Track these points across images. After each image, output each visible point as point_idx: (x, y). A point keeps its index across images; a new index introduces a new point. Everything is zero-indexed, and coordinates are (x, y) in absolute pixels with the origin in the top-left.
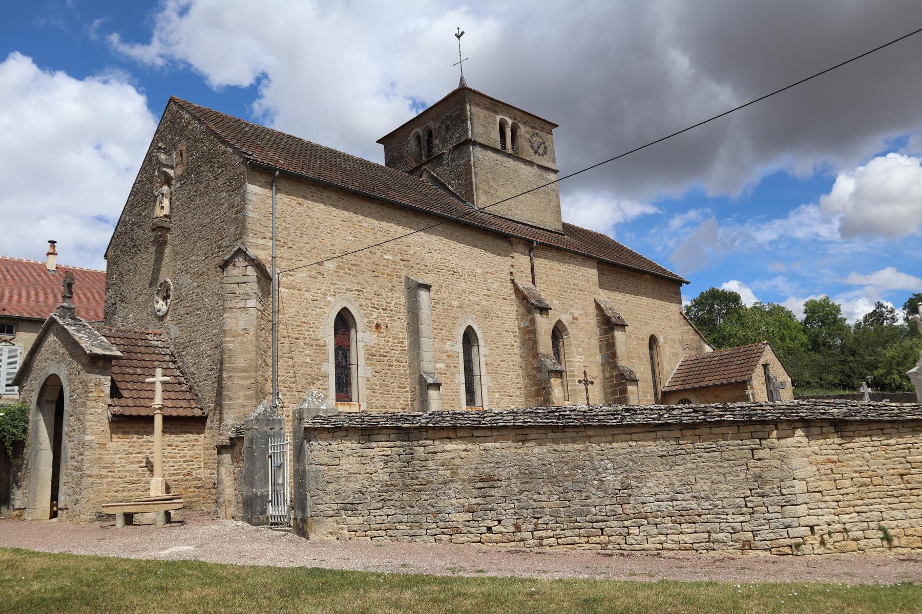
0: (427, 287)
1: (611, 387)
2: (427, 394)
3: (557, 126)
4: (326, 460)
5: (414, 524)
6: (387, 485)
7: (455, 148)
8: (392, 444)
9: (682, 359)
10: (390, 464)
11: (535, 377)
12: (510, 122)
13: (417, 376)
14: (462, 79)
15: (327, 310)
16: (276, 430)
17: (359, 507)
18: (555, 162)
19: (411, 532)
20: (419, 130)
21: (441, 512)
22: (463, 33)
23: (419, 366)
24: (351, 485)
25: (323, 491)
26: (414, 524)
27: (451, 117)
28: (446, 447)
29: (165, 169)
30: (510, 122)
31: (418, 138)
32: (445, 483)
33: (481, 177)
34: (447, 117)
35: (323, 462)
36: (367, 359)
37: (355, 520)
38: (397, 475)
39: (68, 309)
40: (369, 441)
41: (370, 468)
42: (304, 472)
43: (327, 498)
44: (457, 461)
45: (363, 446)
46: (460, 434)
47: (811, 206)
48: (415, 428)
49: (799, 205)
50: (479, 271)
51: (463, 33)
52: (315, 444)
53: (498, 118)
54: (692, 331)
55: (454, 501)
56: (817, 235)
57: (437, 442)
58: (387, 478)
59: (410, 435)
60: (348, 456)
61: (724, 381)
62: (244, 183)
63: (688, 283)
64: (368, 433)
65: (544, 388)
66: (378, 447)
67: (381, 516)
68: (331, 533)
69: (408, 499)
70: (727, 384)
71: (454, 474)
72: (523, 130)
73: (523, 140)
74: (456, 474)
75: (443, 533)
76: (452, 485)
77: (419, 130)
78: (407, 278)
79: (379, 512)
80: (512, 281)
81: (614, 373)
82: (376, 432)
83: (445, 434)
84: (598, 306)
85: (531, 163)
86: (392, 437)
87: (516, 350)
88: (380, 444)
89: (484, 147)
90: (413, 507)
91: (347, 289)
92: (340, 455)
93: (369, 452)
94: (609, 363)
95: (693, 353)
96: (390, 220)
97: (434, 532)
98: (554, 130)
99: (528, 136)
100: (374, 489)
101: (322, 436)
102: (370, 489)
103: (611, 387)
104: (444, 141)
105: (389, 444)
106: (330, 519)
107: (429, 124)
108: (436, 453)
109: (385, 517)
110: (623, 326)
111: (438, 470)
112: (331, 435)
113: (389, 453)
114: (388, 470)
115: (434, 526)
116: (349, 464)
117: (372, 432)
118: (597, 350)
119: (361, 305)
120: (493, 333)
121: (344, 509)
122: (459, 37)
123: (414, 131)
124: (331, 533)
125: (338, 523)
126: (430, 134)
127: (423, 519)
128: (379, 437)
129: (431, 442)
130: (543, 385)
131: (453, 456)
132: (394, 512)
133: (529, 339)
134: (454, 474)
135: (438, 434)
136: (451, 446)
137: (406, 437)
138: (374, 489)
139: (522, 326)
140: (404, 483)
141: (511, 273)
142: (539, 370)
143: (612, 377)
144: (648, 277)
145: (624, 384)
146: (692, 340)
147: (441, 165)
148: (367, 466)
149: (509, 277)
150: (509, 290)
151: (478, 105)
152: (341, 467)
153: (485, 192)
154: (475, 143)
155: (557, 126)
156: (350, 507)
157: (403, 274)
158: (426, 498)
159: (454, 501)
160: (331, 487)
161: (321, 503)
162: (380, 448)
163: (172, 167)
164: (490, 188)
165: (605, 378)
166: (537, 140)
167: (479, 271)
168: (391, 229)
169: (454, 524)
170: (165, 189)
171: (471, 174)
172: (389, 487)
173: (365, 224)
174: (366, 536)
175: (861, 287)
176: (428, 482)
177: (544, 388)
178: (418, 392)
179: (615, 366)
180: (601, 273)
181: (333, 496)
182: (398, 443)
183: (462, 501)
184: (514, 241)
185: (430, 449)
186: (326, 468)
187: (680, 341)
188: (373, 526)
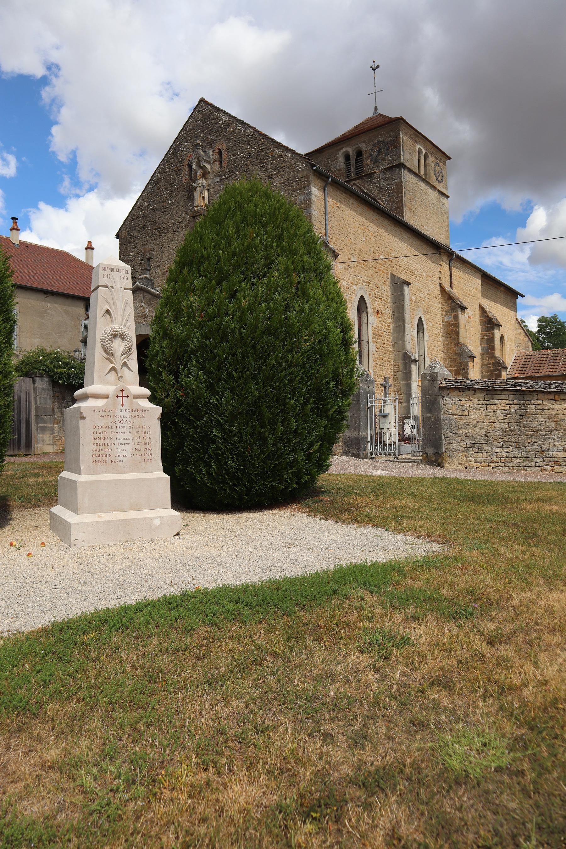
0: (408, 284)
1: (488, 371)
2: (410, 368)
3: (450, 158)
4: (457, 412)
5: (528, 458)
6: (506, 431)
7: (386, 169)
8: (510, 402)
9: (515, 355)
10: (509, 416)
11: (455, 360)
12: (424, 151)
13: (401, 353)
14: (376, 109)
15: (353, 296)
16: (371, 388)
17: (484, 446)
18: (447, 189)
19: (524, 464)
20: (349, 150)
21: (547, 451)
22: (378, 66)
23: (404, 345)
24: (478, 430)
25: (455, 434)
26: (525, 459)
27: (383, 142)
28: (551, 406)
29: (205, 164)
30: (424, 151)
31: (347, 158)
32: (551, 431)
33: (407, 196)
34: (379, 142)
35: (455, 413)
36: (373, 338)
37: (480, 455)
38: (514, 424)
39: (150, 280)
40: (493, 399)
41: (493, 418)
42: (438, 421)
43: (458, 439)
44: (560, 416)
45: (487, 402)
46: (562, 398)
47: (500, 239)
48: (530, 391)
49: (491, 237)
50: (424, 274)
51: (378, 66)
52: (448, 399)
53: (418, 146)
54: (524, 334)
55: (557, 444)
56: (501, 263)
57: (545, 402)
58: (506, 426)
59: (525, 396)
60: (475, 409)
61: (557, 374)
62: (309, 185)
63: (523, 296)
64: (492, 393)
65: (464, 369)
66: (499, 404)
67: (501, 453)
68: (460, 464)
69: (522, 441)
70: (559, 376)
71: (558, 424)
72: (431, 159)
73: (430, 168)
74: (559, 425)
75: (547, 465)
76: (556, 433)
77: (349, 150)
78: (393, 276)
79: (500, 450)
80: (440, 284)
81: (492, 361)
82: (498, 393)
83: (552, 397)
84: (482, 309)
85: (434, 188)
86: (511, 397)
87: (441, 339)
88: (501, 401)
89: (410, 171)
90: (525, 447)
91: (363, 281)
92: (468, 409)
93: (493, 407)
94: (488, 354)
95: (523, 351)
96: (383, 227)
97: (541, 464)
98: (448, 162)
99: (433, 165)
100: (496, 433)
101: (454, 394)
102: (493, 434)
103: (488, 371)
104: (376, 162)
105: (508, 402)
106: (461, 454)
107: (360, 145)
108: (544, 410)
109: (504, 453)
110: (499, 325)
111: (545, 422)
112: (461, 393)
113: (508, 408)
114: (508, 421)
115: (542, 460)
116: (476, 415)
117: (495, 393)
118: (479, 343)
119: (370, 295)
120: (431, 324)
121: (472, 447)
122: (374, 70)
123: (344, 150)
124: (460, 464)
125: (466, 456)
126: (359, 154)
127: (533, 455)
128: (502, 397)
129: (541, 402)
130: (463, 367)
131: (557, 412)
132: (511, 450)
133: (452, 331)
134: (558, 424)
135: (547, 397)
136: (556, 406)
137: (522, 398)
138: (496, 433)
139: (446, 320)
140: (519, 430)
141: (440, 278)
142: (460, 355)
143: (490, 364)
144: (502, 289)
145: (500, 370)
146: (523, 340)
147: (371, 182)
148: (491, 417)
149: (438, 281)
150: (438, 292)
151: (406, 134)
152: (469, 417)
153: (410, 209)
154: (405, 167)
155: (450, 158)
156: (477, 446)
157: (389, 271)
158: (535, 440)
159: (557, 444)
160: (461, 431)
161: (452, 443)
162: (501, 405)
163: (209, 163)
164: (413, 206)
165: (483, 364)
166: (438, 168)
167: (424, 274)
168: (384, 235)
169: (556, 459)
170: (202, 181)
171: (402, 193)
172: (507, 432)
173: (371, 229)
174: (489, 466)
175: (534, 306)
176: (538, 430)
177: (464, 369)
178: (401, 366)
179: (493, 356)
180: (482, 281)
181: (464, 438)
182: (515, 402)
183: (562, 444)
184: (442, 251)
185: (540, 407)
186: (457, 417)
187: (515, 340)
188: (496, 460)
